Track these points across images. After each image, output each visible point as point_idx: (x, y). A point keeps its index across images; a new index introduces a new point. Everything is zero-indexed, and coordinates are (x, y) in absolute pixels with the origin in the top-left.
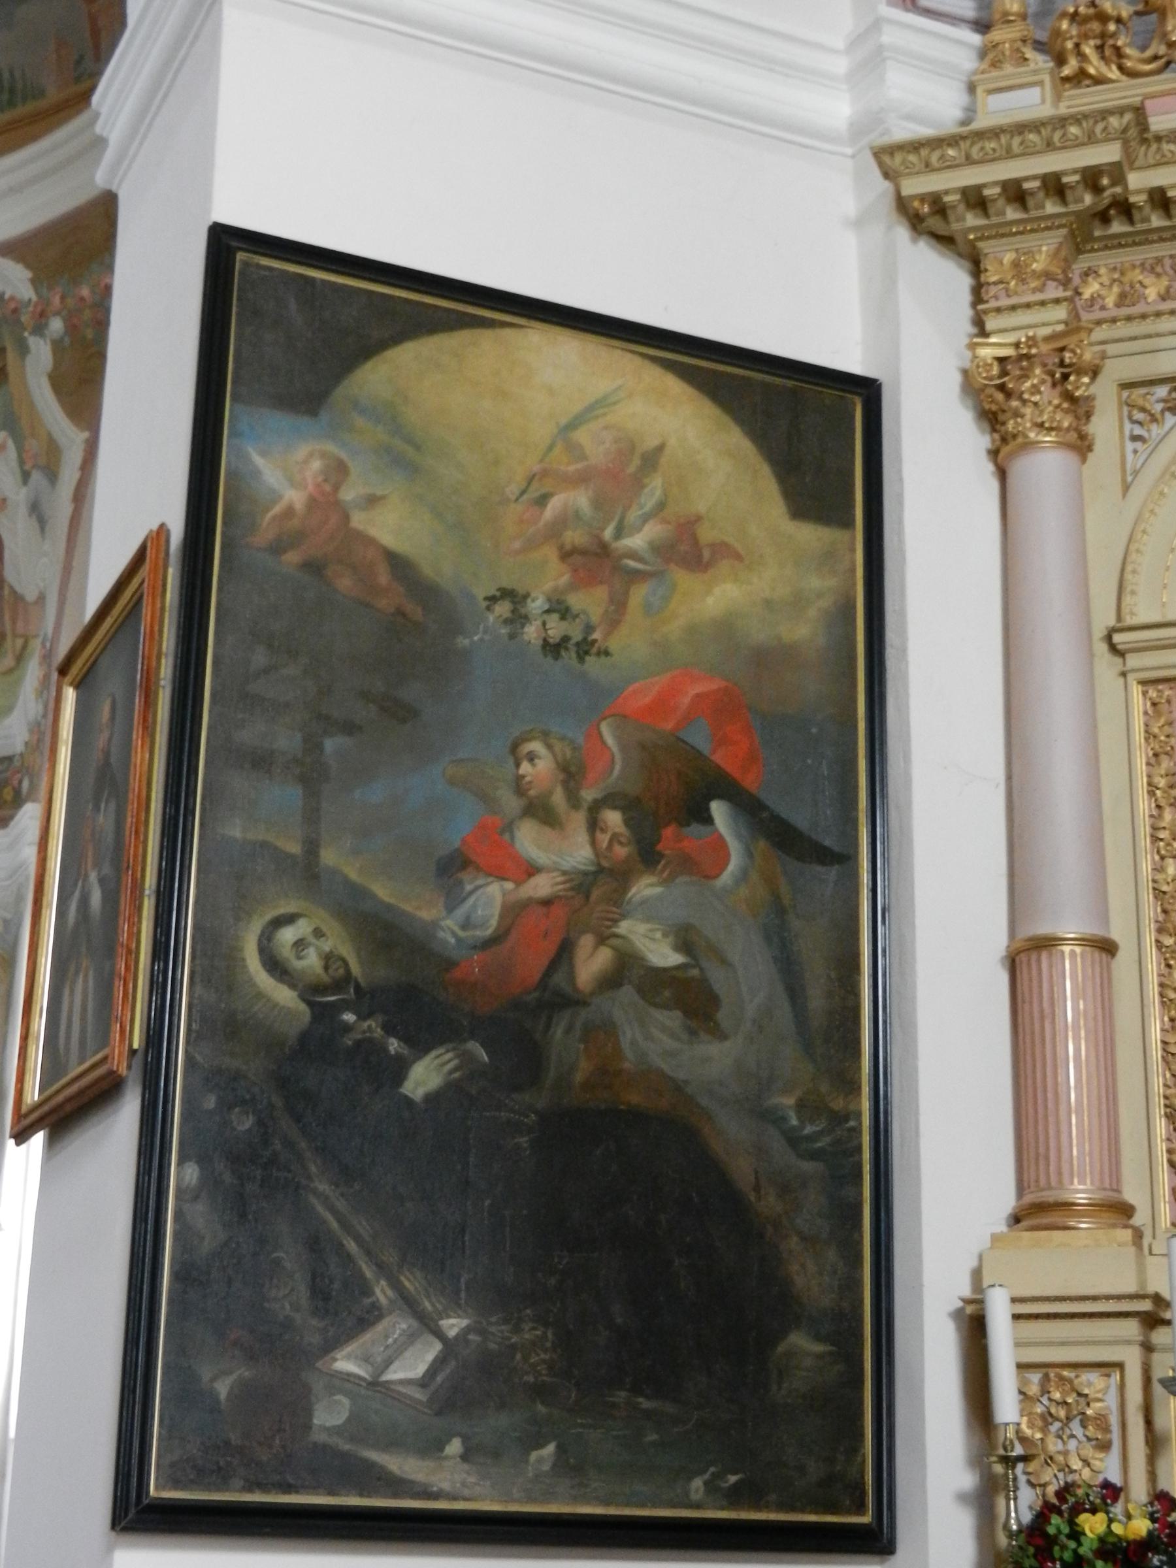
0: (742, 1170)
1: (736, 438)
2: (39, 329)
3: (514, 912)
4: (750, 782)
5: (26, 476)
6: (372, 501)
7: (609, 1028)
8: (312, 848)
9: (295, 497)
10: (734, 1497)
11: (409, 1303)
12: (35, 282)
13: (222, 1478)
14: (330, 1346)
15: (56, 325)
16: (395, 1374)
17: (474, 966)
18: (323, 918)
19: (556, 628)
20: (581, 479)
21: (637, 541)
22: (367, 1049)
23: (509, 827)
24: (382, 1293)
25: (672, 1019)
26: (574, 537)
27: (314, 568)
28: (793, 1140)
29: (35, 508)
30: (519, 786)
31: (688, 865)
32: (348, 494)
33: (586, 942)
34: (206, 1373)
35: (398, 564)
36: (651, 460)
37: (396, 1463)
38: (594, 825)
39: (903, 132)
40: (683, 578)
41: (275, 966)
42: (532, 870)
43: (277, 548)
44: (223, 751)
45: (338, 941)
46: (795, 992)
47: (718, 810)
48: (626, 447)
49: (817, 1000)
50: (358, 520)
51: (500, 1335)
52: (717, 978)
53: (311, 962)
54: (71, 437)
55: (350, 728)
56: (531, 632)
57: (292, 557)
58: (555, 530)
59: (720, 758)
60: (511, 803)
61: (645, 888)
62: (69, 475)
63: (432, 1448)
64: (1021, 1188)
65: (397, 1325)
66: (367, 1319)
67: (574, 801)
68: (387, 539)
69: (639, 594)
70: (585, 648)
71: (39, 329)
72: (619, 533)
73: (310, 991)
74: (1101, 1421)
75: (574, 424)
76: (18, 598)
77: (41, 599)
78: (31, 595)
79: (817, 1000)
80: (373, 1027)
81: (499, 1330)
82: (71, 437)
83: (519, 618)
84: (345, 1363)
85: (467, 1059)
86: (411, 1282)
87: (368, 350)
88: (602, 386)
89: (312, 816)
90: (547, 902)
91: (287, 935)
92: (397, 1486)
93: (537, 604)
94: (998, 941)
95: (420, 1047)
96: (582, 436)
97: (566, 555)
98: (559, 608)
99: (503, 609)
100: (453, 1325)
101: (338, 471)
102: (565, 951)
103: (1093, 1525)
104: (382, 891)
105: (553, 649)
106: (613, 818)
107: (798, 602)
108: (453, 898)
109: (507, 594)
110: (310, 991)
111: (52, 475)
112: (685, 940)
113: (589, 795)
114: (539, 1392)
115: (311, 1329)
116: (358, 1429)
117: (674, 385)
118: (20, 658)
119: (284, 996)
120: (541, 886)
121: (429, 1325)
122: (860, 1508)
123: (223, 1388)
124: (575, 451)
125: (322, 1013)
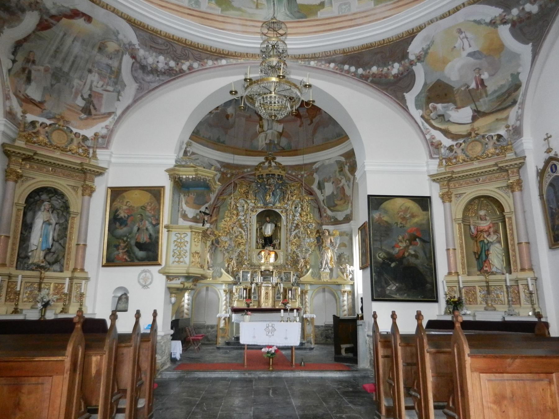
0: (422, 270)
1: (417, 205)
2: (346, 165)
3: (399, 251)
4: (420, 236)
5: (346, 182)
6: (383, 217)
7: (409, 260)
8: (381, 248)
9: (377, 217)
10: (423, 298)
11: (393, 283)
12: (345, 159)
13: (379, 297)
14: (387, 287)
15: (348, 164)
16: (392, 289)
17: (396, 255)
18: (383, 253)
19: (401, 225)
20: (402, 211)
21: (408, 216)
22: (388, 263)
23: (398, 243)
24: (391, 282)
25: (414, 258)
26: (402, 217)
27: (379, 223)
28: (426, 268)
29: (348, 185)
30: (399, 240)
31: (414, 245)
32: (381, 216)
33: (406, 252)
34: (377, 289)
35: (386, 222)
36: (409, 208)
37: (393, 296)
38: (406, 242)
39: (431, 174)
40: (413, 219)
41: (379, 257)
42: (401, 247)
43: (376, 222)
44: (374, 240)
45: (384, 255)
46: (425, 254)
47: (417, 239)
48: (406, 208)
49: (428, 255)
50: (383, 219)
51: (496, 168)
52: (418, 254)
53: (382, 256)
54: (352, 177)
55: (384, 237)
56: (399, 226)
57: (377, 223)
58: (400, 216)
59: (417, 234)
60: (398, 241)
61: (411, 247)
62: (352, 181)
63: (396, 294)
64: (449, 270)
65: (393, 285)
66: (390, 285)
67: (404, 240)
68: (385, 220)
69: (408, 221)
70: (404, 227)
71: (346, 165)
72: (406, 215)
73: (382, 259)
74: (455, 291)
75: (401, 206)
76: (347, 196)
77: (350, 196)
78: (349, 195)
79: (428, 255)
80: (388, 261)
81: (401, 285)
82: (352, 177)
83: (397, 225)
84: (388, 288)
85: (396, 264)
86: (393, 282)
87: (382, 203)
88: (403, 202)
89: (381, 244)
90: (402, 249)
91: (380, 254)
92: (393, 297)
93: (399, 223)
94: (445, 248)
95: (392, 262)
96: (402, 207)
97: (401, 218)
98: (401, 224)
99: (396, 224)
100: (397, 285)
101: (380, 215)
102: (404, 254)
103: (452, 300)
104: (388, 250)
105: (401, 227)
106: (407, 241)
107: (424, 219)
108: (394, 250)
109: (396, 223)
110: (382, 259)
111: (350, 181)
112: (415, 251)
113: (405, 239)
114: (405, 290)
115: (385, 286)
116: (390, 293)
117: (410, 201)
118: (348, 203)
119: (380, 259)
120: (401, 248)
121: (395, 285)
122: (474, 287)
123: (379, 290)
124: (401, 209)
125: (384, 261)
